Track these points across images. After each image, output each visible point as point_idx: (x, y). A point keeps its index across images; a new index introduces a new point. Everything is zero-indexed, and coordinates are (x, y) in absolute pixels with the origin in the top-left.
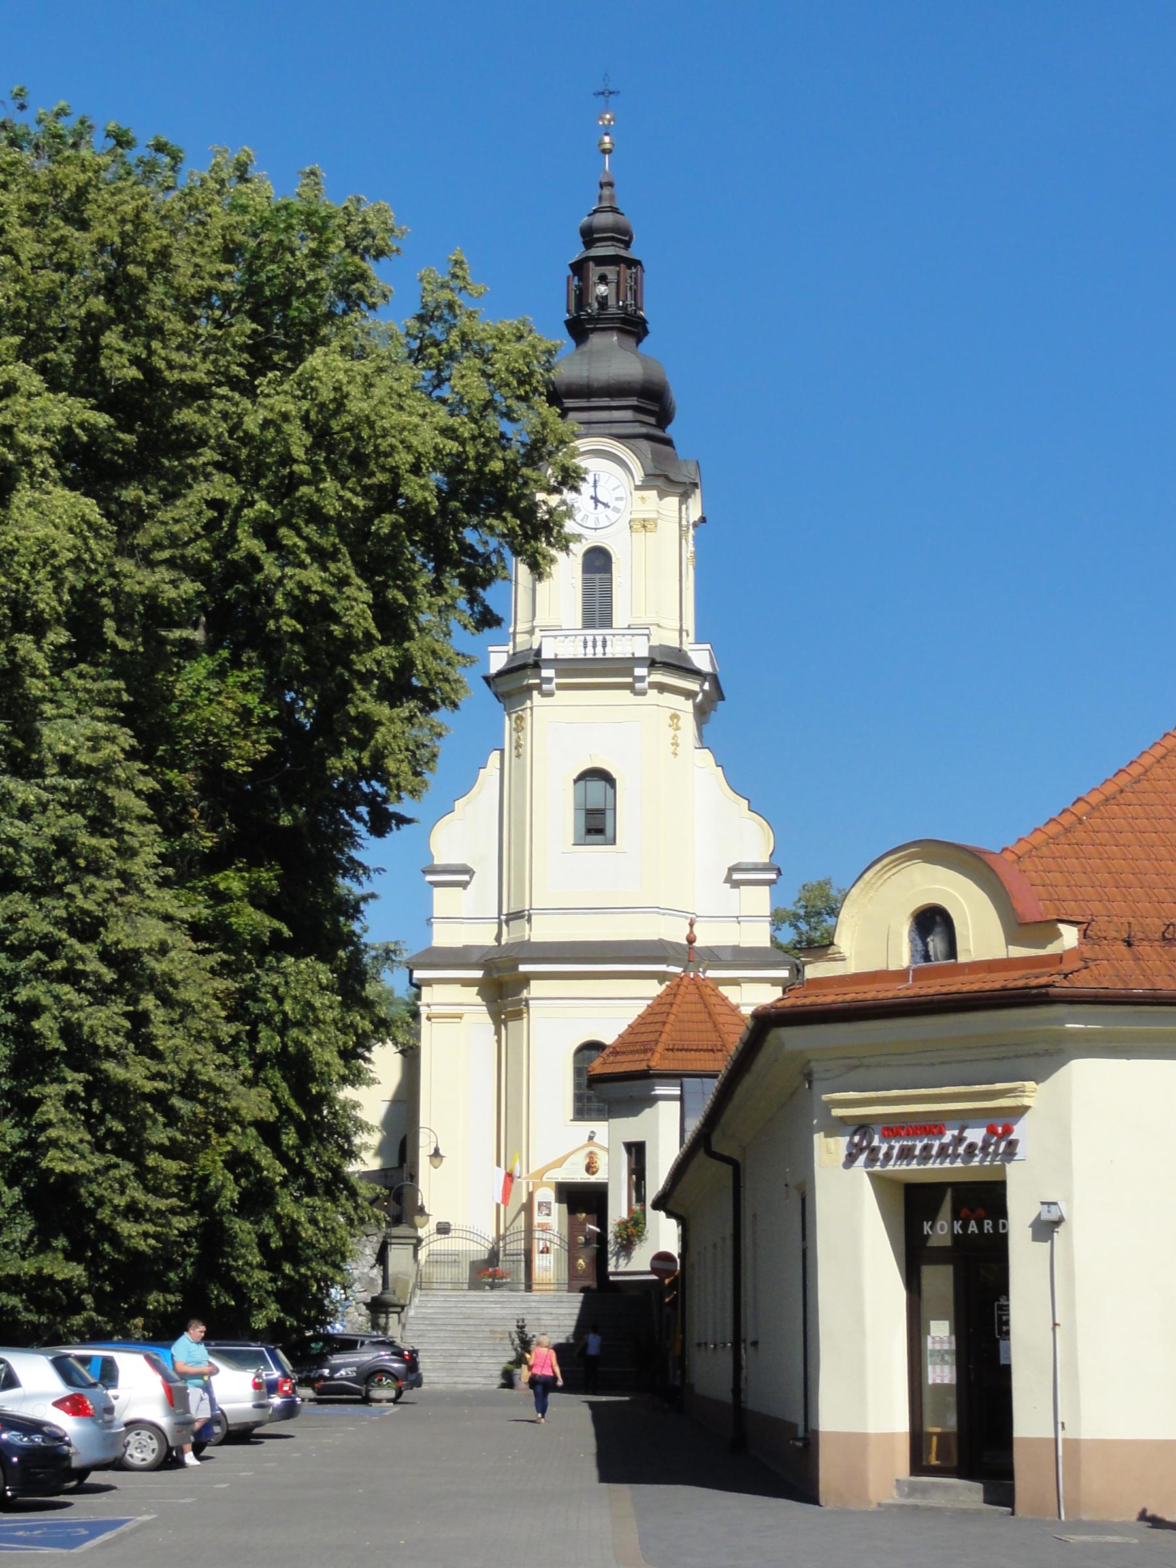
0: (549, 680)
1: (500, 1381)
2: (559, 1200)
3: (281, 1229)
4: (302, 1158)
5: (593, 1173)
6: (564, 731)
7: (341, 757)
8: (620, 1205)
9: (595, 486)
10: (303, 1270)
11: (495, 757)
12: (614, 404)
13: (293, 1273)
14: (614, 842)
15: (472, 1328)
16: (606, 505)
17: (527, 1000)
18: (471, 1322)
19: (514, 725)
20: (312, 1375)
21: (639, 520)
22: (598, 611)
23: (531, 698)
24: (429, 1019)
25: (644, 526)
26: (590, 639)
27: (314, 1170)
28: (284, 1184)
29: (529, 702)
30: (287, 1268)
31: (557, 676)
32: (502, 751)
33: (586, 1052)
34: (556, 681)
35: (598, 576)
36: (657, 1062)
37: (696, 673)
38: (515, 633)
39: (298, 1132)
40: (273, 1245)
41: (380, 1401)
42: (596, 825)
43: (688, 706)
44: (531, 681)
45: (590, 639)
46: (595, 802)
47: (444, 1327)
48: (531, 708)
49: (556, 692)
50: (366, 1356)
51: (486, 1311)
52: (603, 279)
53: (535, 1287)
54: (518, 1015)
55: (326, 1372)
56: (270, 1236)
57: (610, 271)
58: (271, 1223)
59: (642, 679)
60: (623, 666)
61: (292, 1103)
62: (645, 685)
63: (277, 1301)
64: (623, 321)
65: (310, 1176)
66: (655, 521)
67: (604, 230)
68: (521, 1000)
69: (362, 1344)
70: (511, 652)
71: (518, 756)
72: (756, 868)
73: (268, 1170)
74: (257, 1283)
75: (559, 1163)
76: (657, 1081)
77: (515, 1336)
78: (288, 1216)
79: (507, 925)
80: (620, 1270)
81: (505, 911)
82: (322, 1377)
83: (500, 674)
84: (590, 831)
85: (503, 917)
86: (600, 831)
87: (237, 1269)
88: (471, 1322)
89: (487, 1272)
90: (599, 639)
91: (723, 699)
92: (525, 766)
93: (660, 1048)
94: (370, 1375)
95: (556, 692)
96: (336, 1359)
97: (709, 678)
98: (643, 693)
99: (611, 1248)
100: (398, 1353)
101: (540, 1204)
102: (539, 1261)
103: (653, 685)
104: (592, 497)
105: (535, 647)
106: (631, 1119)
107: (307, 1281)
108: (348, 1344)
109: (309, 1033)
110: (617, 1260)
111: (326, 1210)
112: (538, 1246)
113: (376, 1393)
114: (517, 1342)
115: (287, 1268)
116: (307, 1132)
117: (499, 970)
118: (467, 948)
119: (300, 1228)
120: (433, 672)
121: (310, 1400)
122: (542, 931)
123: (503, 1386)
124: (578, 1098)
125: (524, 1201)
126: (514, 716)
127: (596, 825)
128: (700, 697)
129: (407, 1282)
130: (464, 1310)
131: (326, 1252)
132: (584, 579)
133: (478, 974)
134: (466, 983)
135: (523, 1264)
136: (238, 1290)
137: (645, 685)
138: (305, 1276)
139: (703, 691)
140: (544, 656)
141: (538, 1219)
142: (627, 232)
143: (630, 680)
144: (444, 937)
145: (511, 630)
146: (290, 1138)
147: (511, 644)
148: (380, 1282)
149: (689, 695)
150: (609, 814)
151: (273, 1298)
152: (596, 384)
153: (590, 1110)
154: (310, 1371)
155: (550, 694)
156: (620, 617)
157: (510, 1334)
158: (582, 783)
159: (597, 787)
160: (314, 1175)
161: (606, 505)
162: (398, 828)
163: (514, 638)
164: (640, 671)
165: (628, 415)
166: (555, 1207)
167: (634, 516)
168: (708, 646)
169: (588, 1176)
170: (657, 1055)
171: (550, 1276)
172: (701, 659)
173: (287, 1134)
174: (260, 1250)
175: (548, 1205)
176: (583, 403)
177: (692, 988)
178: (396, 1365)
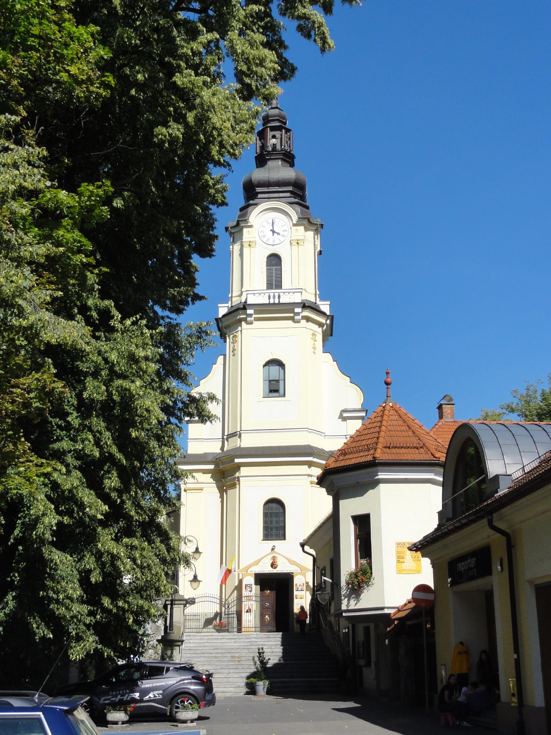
0: (251, 315)
1: (245, 690)
2: (256, 584)
3: (103, 565)
4: (123, 502)
5: (275, 568)
6: (256, 341)
7: (167, 127)
8: (350, 557)
9: (273, 225)
10: (120, 604)
11: (221, 359)
12: (280, 190)
13: (111, 607)
14: (284, 396)
15: (220, 655)
16: (278, 234)
17: (238, 478)
18: (219, 651)
19: (231, 341)
20: (125, 698)
21: (295, 240)
22: (274, 281)
23: (241, 326)
24: (185, 491)
25: (298, 243)
26: (272, 295)
27: (133, 513)
28: (104, 524)
29: (240, 328)
30: (106, 602)
31: (255, 314)
32: (225, 355)
33: (270, 505)
34: (254, 316)
35: (274, 268)
36: (381, 455)
37: (324, 314)
38: (232, 297)
39: (119, 476)
40: (93, 580)
41: (184, 722)
42: (275, 388)
43: (320, 330)
44: (241, 316)
45: (272, 295)
46: (274, 376)
47: (202, 655)
48: (241, 331)
49: (254, 322)
50: (171, 680)
51: (226, 644)
52: (274, 137)
53: (243, 630)
54: (233, 486)
55: (137, 695)
56: (89, 571)
57: (277, 134)
58: (93, 559)
59: (298, 314)
60: (289, 307)
61: (114, 450)
62: (300, 317)
63: (96, 633)
64: (284, 155)
65: (129, 518)
66: (303, 240)
67: (274, 116)
68: (235, 478)
69: (168, 670)
70: (230, 306)
71: (234, 355)
72: (355, 411)
73: (90, 507)
74: (74, 617)
75: (257, 563)
76: (380, 468)
77: (256, 659)
78: (109, 553)
79: (227, 441)
80: (350, 608)
81: (226, 434)
82: (134, 701)
83: (224, 316)
84: (271, 391)
85: (225, 437)
86: (277, 391)
87: (57, 601)
88: (219, 651)
89: (217, 623)
90: (277, 295)
91: (331, 335)
92: (237, 361)
93: (380, 446)
94: (175, 697)
95: (254, 322)
96: (146, 684)
97: (330, 318)
98: (298, 322)
99: (343, 592)
100: (197, 677)
101: (246, 586)
102: (245, 617)
103: (304, 318)
104: (271, 230)
105: (243, 301)
106: (357, 499)
107: (124, 614)
108: (155, 671)
109: (133, 382)
110: (349, 600)
111: (143, 549)
112: (244, 609)
113: (182, 715)
114: (258, 662)
115: (106, 602)
116: (128, 476)
117: (223, 463)
118: (205, 454)
119: (119, 563)
120: (251, 57)
121: (123, 723)
122: (248, 441)
123: (247, 693)
124: (266, 528)
125: (236, 584)
126: (231, 336)
127: (275, 388)
128: (325, 327)
129: (180, 628)
130: (212, 644)
131: (142, 588)
132: (267, 269)
133: (212, 467)
134: (205, 472)
135: (236, 619)
136: (56, 623)
137: (300, 317)
138: (123, 608)
139: (326, 324)
140: (248, 303)
141: (245, 593)
142: (284, 118)
143: (292, 315)
144: (193, 448)
145: (230, 296)
146: (112, 481)
147: (230, 302)
148: (163, 628)
149: (320, 325)
150: (281, 383)
151: (92, 631)
152: (272, 180)
153: (271, 535)
154: (123, 695)
155: (251, 323)
156: (286, 283)
157: (253, 658)
158: (267, 367)
159: (275, 369)
160: (132, 517)
161: (278, 234)
162: (193, 304)
163: (232, 299)
164: (298, 310)
165: (288, 195)
166: (254, 587)
167: (292, 238)
168: (329, 303)
169: (272, 569)
170: (379, 451)
171: (252, 624)
172: (325, 307)
173: (110, 478)
174: (81, 586)
175: (250, 586)
176: (266, 190)
177: (392, 412)
178: (192, 687)
